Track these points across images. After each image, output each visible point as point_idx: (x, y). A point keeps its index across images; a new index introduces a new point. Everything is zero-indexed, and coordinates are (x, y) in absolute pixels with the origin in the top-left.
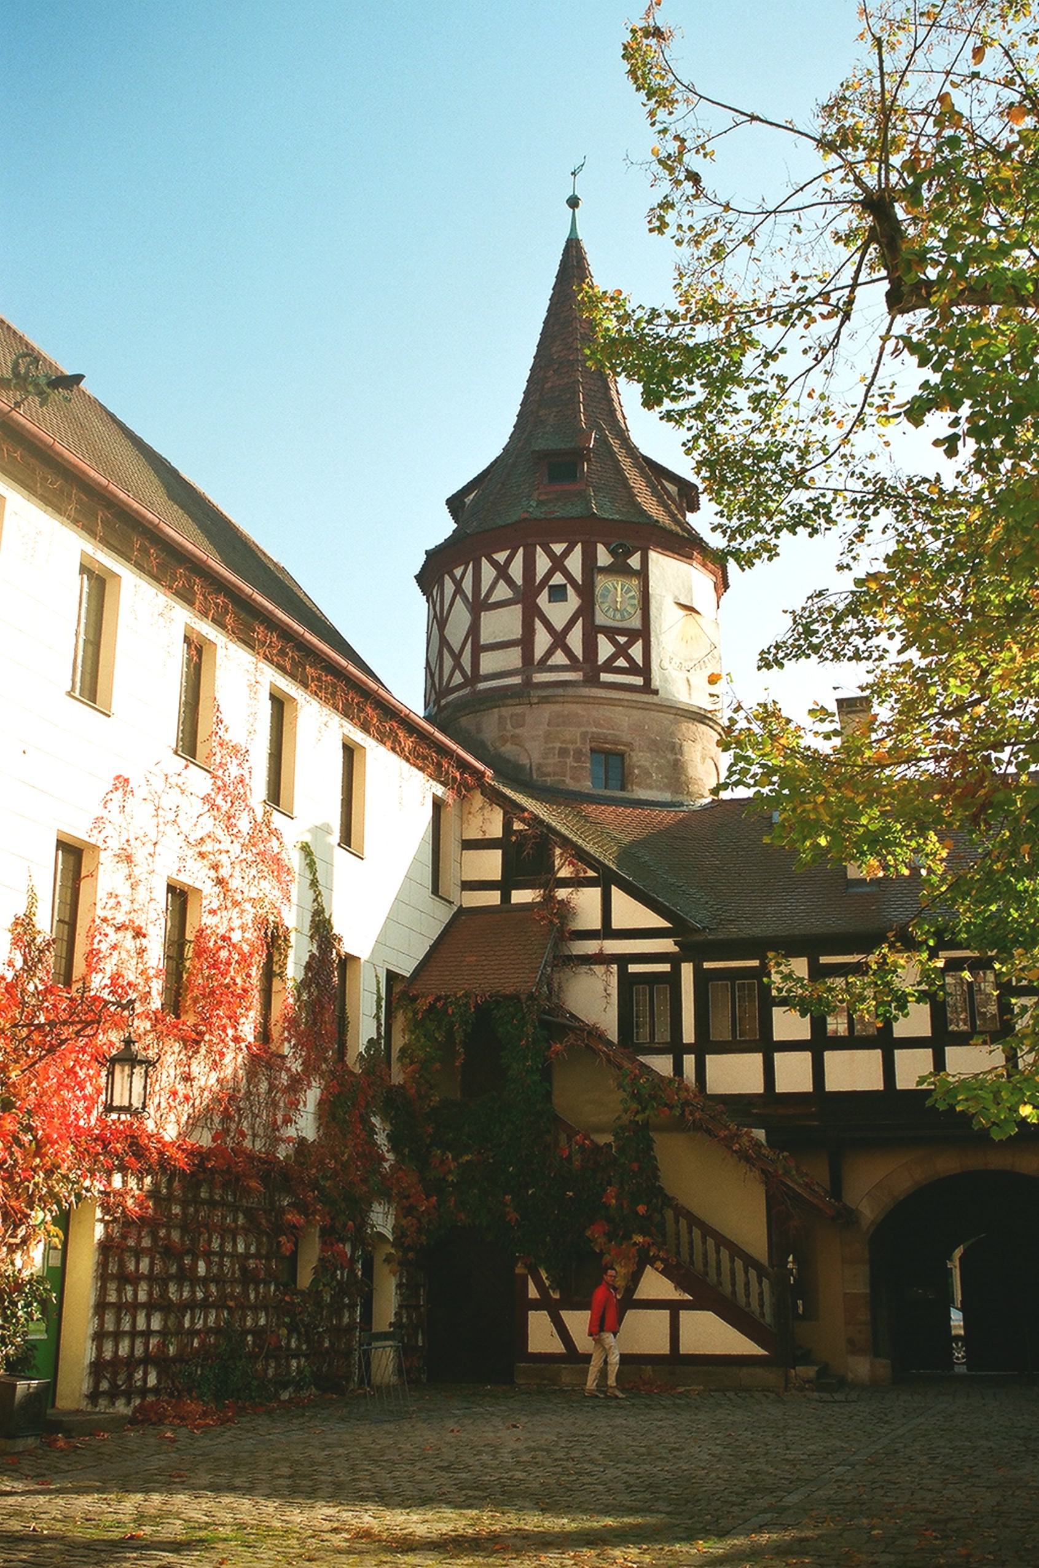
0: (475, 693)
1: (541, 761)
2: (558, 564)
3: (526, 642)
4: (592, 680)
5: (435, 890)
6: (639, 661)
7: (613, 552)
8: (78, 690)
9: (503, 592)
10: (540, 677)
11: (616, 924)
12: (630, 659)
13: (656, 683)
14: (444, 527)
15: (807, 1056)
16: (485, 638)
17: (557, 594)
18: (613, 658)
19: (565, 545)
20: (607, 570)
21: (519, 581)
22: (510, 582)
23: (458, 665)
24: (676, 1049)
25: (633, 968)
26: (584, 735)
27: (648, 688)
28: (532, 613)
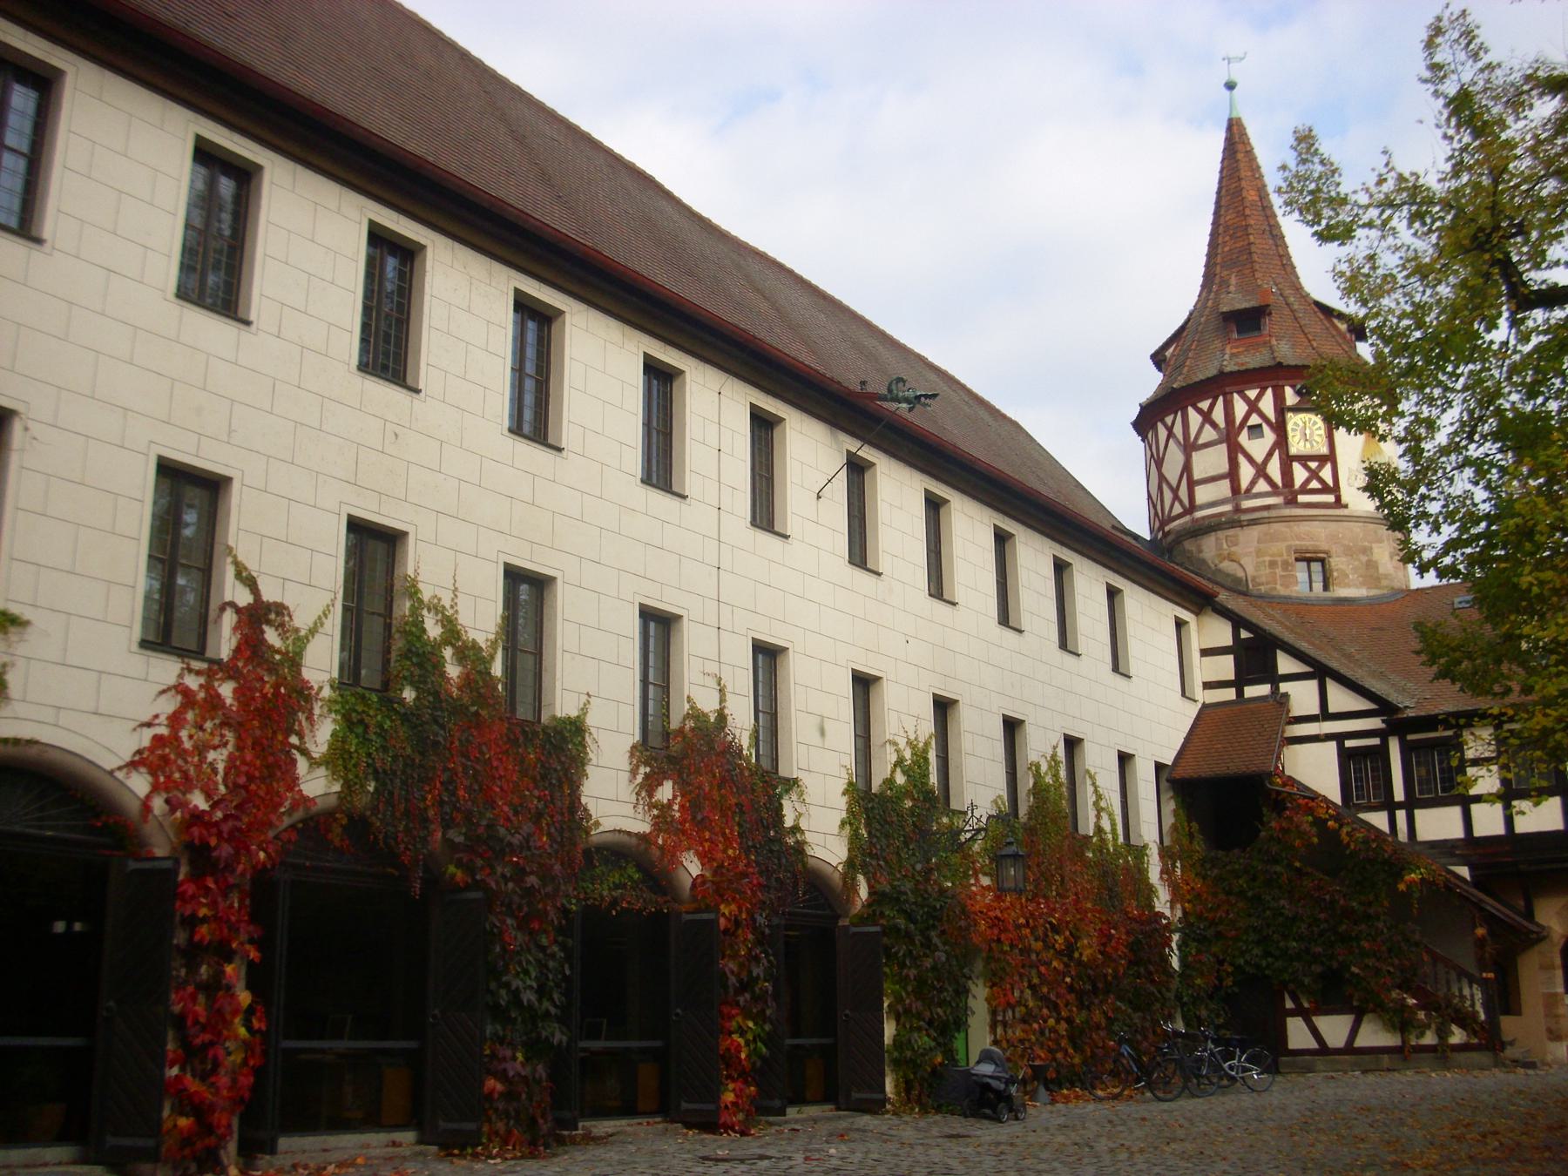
0: (1195, 521)
1: (1255, 574)
2: (1253, 407)
3: (1233, 474)
4: (1291, 501)
5: (1183, 694)
6: (1330, 482)
7: (1298, 393)
8: (765, 523)
9: (1209, 434)
10: (1247, 504)
11: (1332, 709)
12: (1321, 481)
13: (1344, 499)
14: (1150, 382)
15: (1499, 807)
16: (1198, 474)
17: (1256, 431)
18: (1308, 481)
19: (1257, 391)
20: (1296, 409)
21: (1222, 424)
22: (1214, 425)
23: (1176, 497)
24: (1390, 807)
25: (1349, 743)
26: (1289, 548)
27: (1338, 503)
28: (1235, 450)
